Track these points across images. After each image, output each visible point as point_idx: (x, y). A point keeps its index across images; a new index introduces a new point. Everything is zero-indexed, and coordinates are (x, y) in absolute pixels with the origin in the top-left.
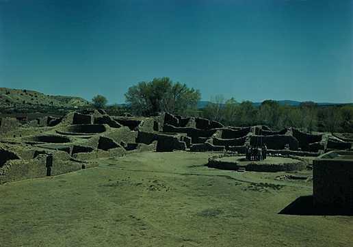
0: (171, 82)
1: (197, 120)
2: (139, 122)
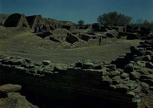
0: (117, 13)
1: (141, 27)
2: (118, 28)
